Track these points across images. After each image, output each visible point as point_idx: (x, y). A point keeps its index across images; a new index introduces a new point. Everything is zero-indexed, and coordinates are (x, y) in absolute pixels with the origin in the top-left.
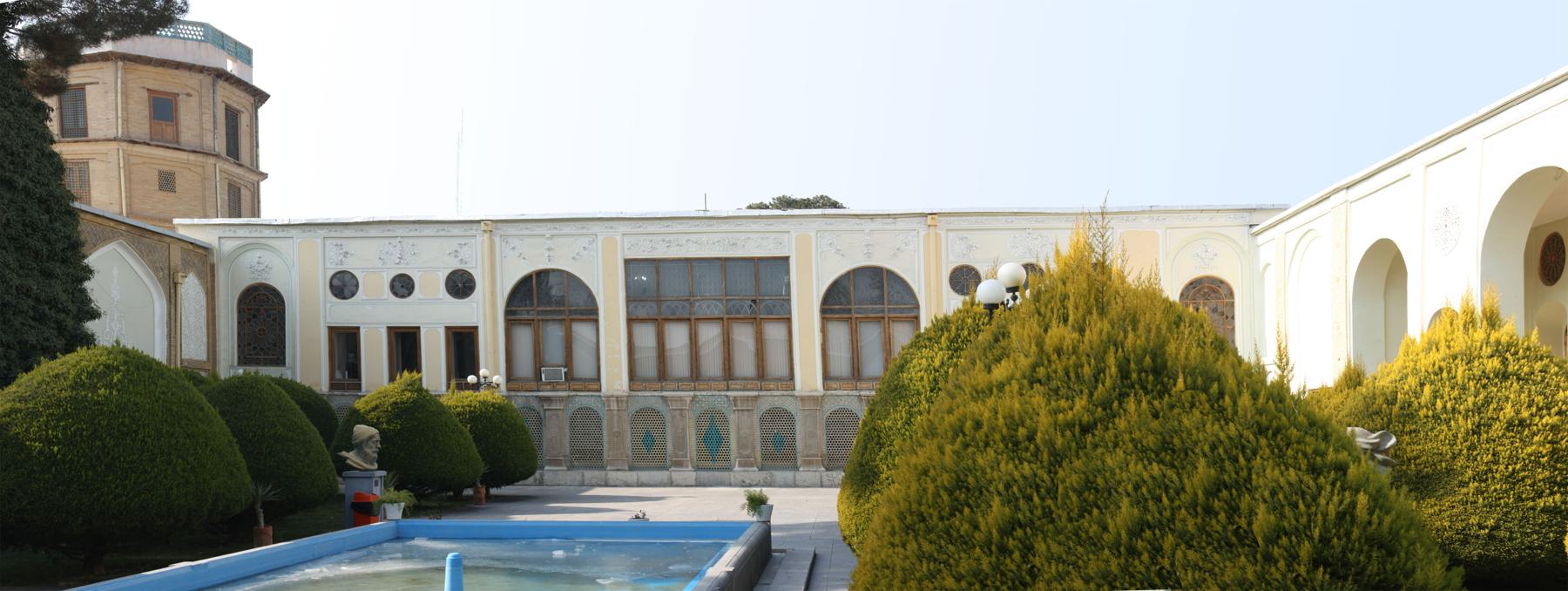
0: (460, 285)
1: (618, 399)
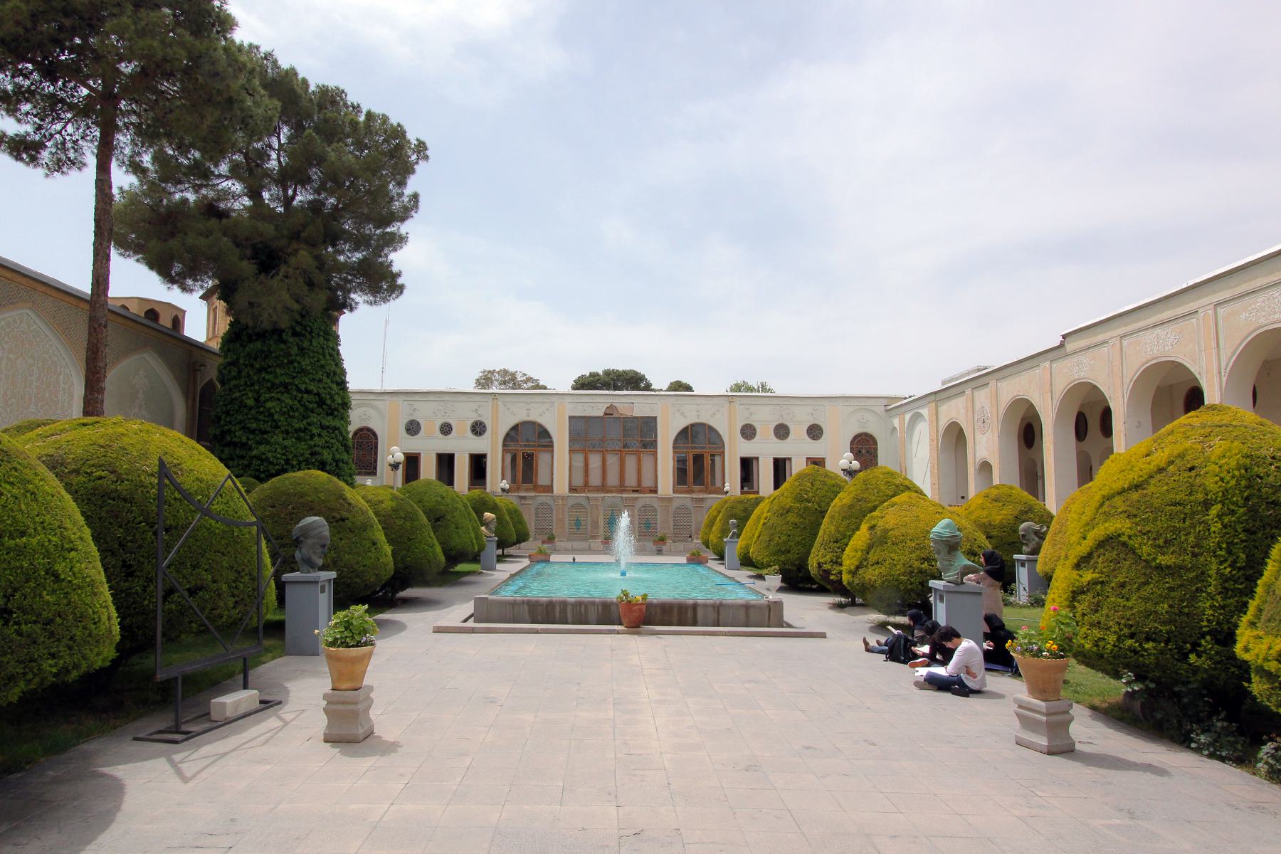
0: (478, 429)
1: (563, 498)
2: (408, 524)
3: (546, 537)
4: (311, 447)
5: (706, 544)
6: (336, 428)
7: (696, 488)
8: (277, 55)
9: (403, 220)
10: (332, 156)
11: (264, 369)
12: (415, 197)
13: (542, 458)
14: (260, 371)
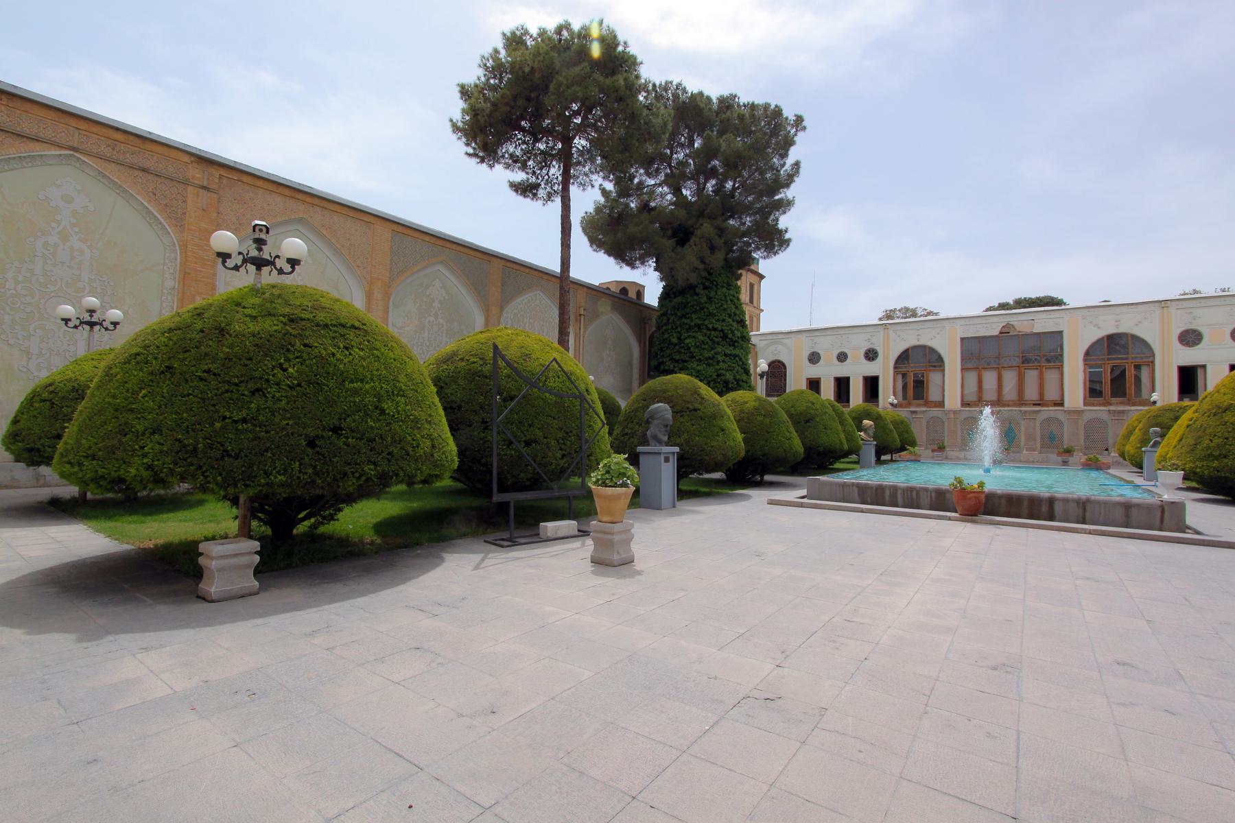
0: (871, 355)
1: (955, 412)
2: (768, 420)
3: (936, 447)
4: (717, 370)
5: (1122, 455)
6: (736, 356)
7: (1114, 400)
8: (685, 84)
9: (787, 186)
10: (724, 146)
11: (683, 316)
12: (797, 165)
13: (934, 378)
14: (681, 318)
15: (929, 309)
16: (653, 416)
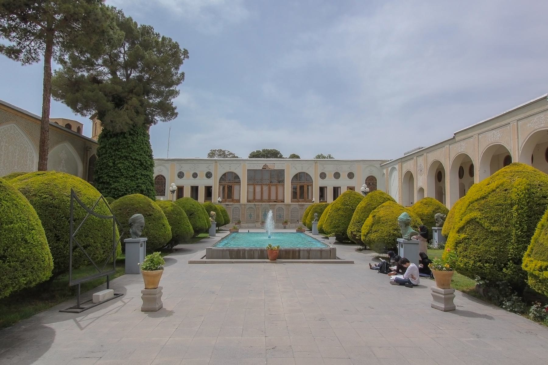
0: (209, 175)
3: (237, 222)
4: (137, 184)
6: (148, 175)
7: (300, 200)
9: (177, 84)
12: (183, 74)
13: (236, 188)
14: (115, 150)
15: (231, 151)
16: (134, 221)
